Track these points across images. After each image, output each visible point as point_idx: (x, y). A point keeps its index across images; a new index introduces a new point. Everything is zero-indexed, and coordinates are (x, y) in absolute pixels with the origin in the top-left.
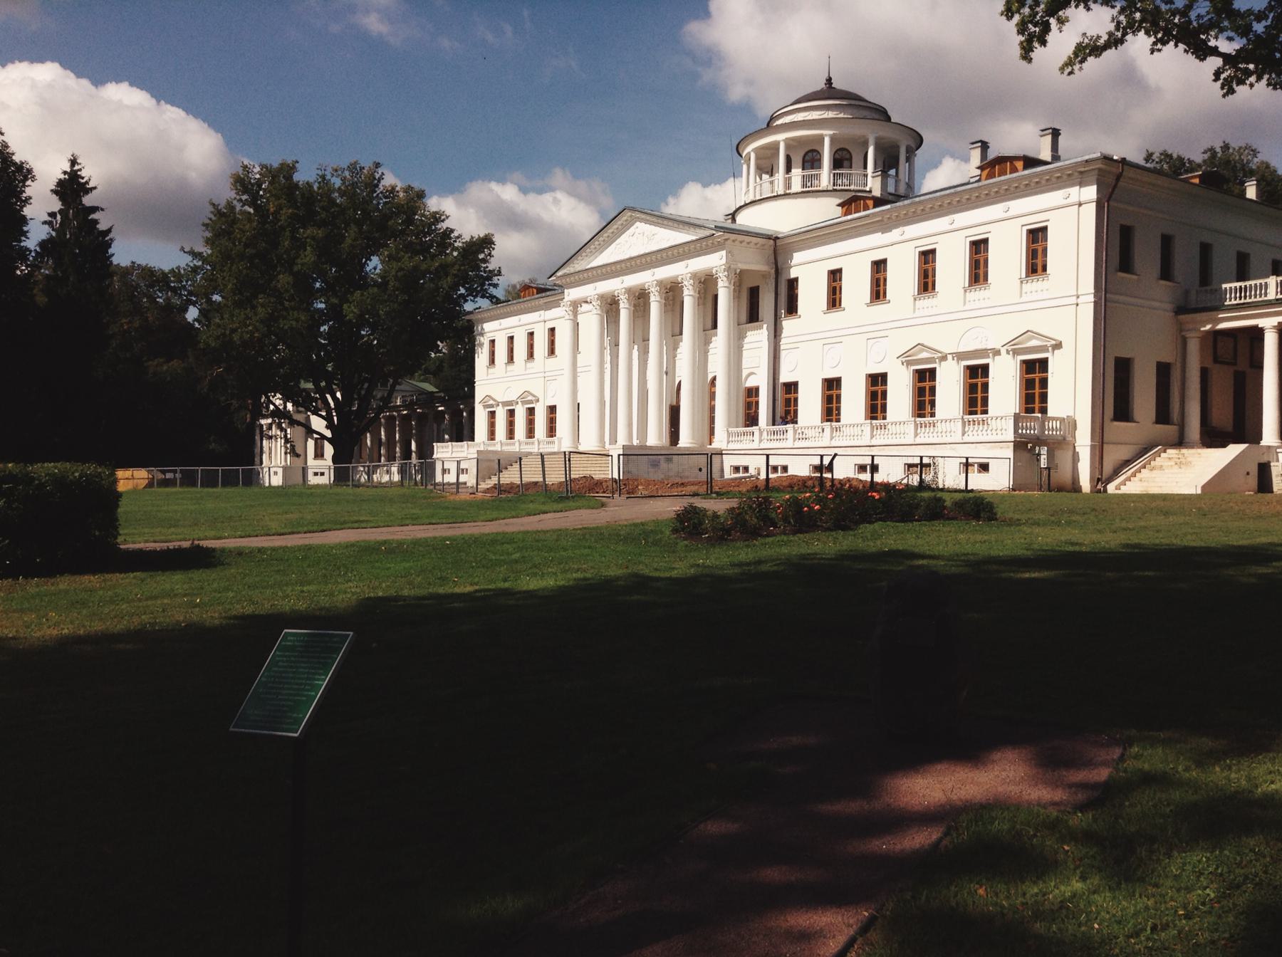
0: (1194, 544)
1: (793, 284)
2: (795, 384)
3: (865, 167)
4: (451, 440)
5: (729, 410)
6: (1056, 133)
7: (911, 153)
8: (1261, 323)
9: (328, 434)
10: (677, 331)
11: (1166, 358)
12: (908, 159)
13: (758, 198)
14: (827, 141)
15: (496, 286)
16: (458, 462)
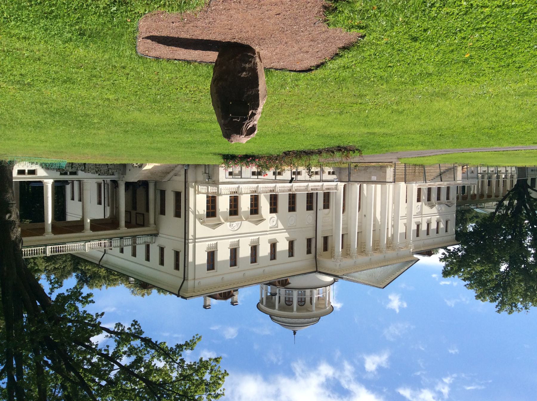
1: (309, 252)
4: (456, 231)
5: (48, 213)
6: (205, 307)
7: (261, 301)
8: (52, 236)
9: (529, 190)
10: (345, 236)
11: (163, 216)
12: (262, 299)
14: (295, 309)
15: (443, 254)
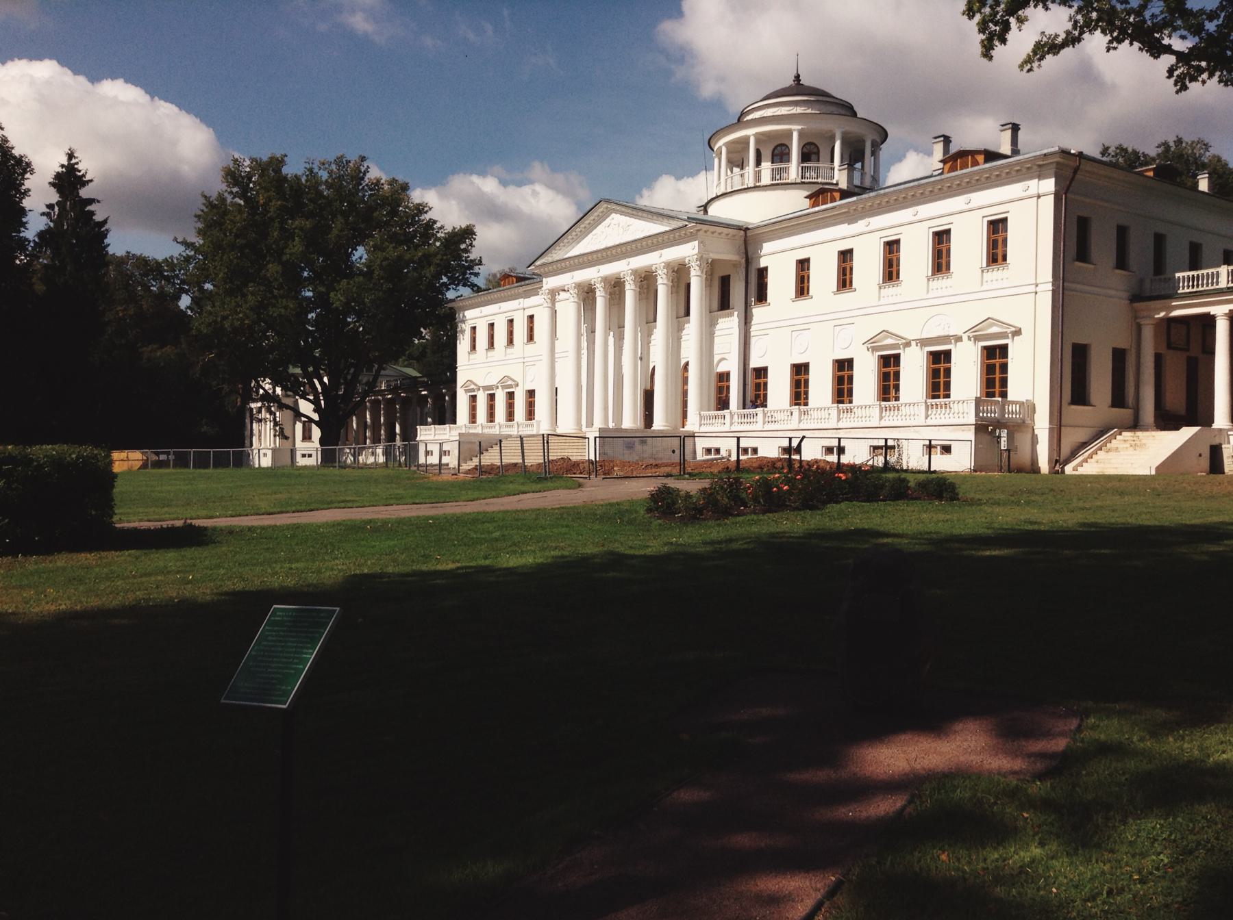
0: (1148, 523)
1: (762, 273)
2: (765, 370)
3: (832, 161)
5: (701, 394)
6: (1015, 128)
7: (876, 147)
8: (1213, 310)
9: (316, 417)
10: (652, 319)
11: (1122, 344)
12: (873, 153)
13: (729, 190)
14: (795, 136)
15: (477, 275)
16: (441, 445)
